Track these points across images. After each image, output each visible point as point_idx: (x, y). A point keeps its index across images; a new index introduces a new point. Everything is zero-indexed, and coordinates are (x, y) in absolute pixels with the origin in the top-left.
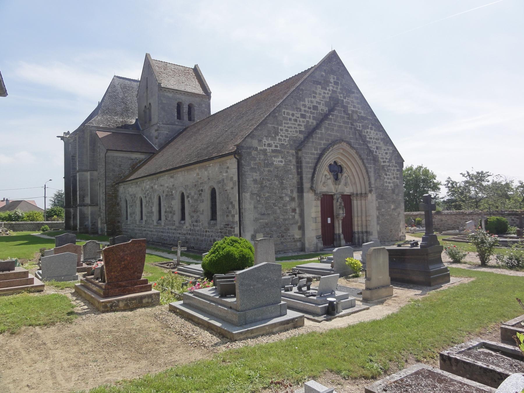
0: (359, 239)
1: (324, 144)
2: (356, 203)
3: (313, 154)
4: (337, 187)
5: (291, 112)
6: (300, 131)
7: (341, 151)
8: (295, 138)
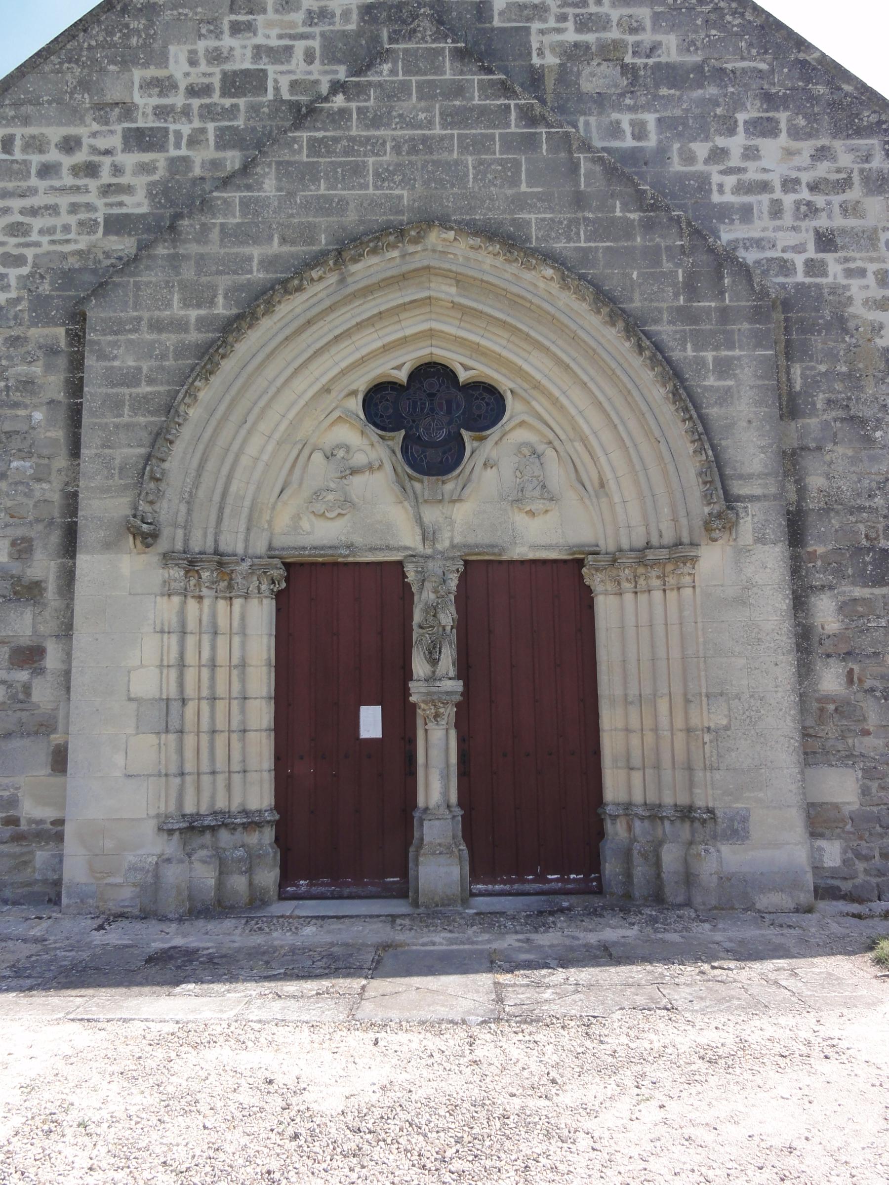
0: (627, 855)
1: (268, 263)
2: (133, 696)
3: (180, 326)
4: (431, 515)
5: (55, 133)
6: (108, 219)
7: (446, 291)
8: (74, 262)
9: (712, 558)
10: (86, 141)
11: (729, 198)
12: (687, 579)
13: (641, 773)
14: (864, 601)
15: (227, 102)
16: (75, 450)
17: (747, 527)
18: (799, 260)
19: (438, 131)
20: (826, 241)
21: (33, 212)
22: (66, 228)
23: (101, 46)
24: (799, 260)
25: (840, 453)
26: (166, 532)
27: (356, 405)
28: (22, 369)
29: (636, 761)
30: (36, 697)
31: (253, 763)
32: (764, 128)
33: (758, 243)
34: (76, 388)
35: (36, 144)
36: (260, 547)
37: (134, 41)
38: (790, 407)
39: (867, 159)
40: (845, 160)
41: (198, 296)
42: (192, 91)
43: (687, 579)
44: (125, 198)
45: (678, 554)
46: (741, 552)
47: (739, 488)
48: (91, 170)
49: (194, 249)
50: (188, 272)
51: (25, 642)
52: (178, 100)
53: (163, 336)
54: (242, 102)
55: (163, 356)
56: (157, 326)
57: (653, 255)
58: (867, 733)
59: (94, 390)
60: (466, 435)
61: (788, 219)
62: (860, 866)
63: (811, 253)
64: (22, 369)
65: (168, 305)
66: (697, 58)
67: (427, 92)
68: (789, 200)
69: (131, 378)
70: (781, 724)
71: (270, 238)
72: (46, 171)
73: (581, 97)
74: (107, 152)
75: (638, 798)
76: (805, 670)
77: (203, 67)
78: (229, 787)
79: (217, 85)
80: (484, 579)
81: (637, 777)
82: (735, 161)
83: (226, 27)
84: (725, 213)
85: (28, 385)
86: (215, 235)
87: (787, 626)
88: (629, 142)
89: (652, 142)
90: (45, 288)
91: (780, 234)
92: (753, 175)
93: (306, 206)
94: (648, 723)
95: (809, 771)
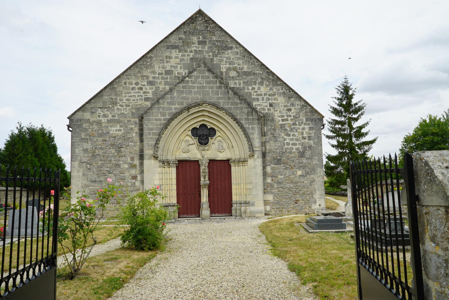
3: (160, 120)
4: (203, 152)
5: (134, 82)
9: (251, 162)
10: (140, 83)
11: (255, 97)
12: (246, 164)
13: (13, 193)
14: (275, 168)
15: (166, 76)
16: (142, 141)
17: (256, 156)
18: (266, 108)
19: (205, 85)
20: (271, 105)
21: (131, 96)
22: (137, 100)
23: (142, 65)
24: (266, 108)
25: (272, 143)
26: (159, 157)
27: (190, 133)
28: (130, 126)
29: (238, 194)
30: (136, 184)
31: (174, 196)
32: (261, 83)
33: (259, 105)
34: (141, 130)
35: (131, 83)
36: (174, 158)
37: (148, 64)
38: (263, 134)
39: (279, 90)
40: (275, 90)
41: (163, 114)
42: (159, 74)
43: (246, 164)
44: (148, 94)
45: (244, 161)
46: (255, 160)
47: (255, 149)
48: (141, 89)
49: (163, 106)
50: (161, 110)
51: (134, 175)
52: (157, 75)
53: (157, 122)
54: (168, 76)
55: (157, 125)
56: (156, 120)
57: (241, 109)
58: (274, 189)
59: (146, 131)
60: (209, 138)
61: (265, 101)
62: (273, 210)
63: (268, 107)
64: (130, 126)
65: (158, 116)
66: (250, 70)
67: (203, 77)
68: (265, 97)
69: (152, 129)
70: (260, 188)
71: (176, 104)
72: (133, 89)
73: (230, 77)
74: (144, 85)
75: (238, 200)
76: (264, 179)
77: (161, 69)
78: (170, 199)
79: (164, 73)
80: (212, 162)
81: (238, 197)
82: (256, 90)
83: (165, 62)
84: (254, 99)
85: (131, 129)
86: (166, 103)
87: (262, 172)
88: (238, 86)
89: (242, 86)
90: (134, 111)
91: (263, 104)
92: (259, 93)
93: (182, 98)
94: (240, 188)
95: (265, 195)
